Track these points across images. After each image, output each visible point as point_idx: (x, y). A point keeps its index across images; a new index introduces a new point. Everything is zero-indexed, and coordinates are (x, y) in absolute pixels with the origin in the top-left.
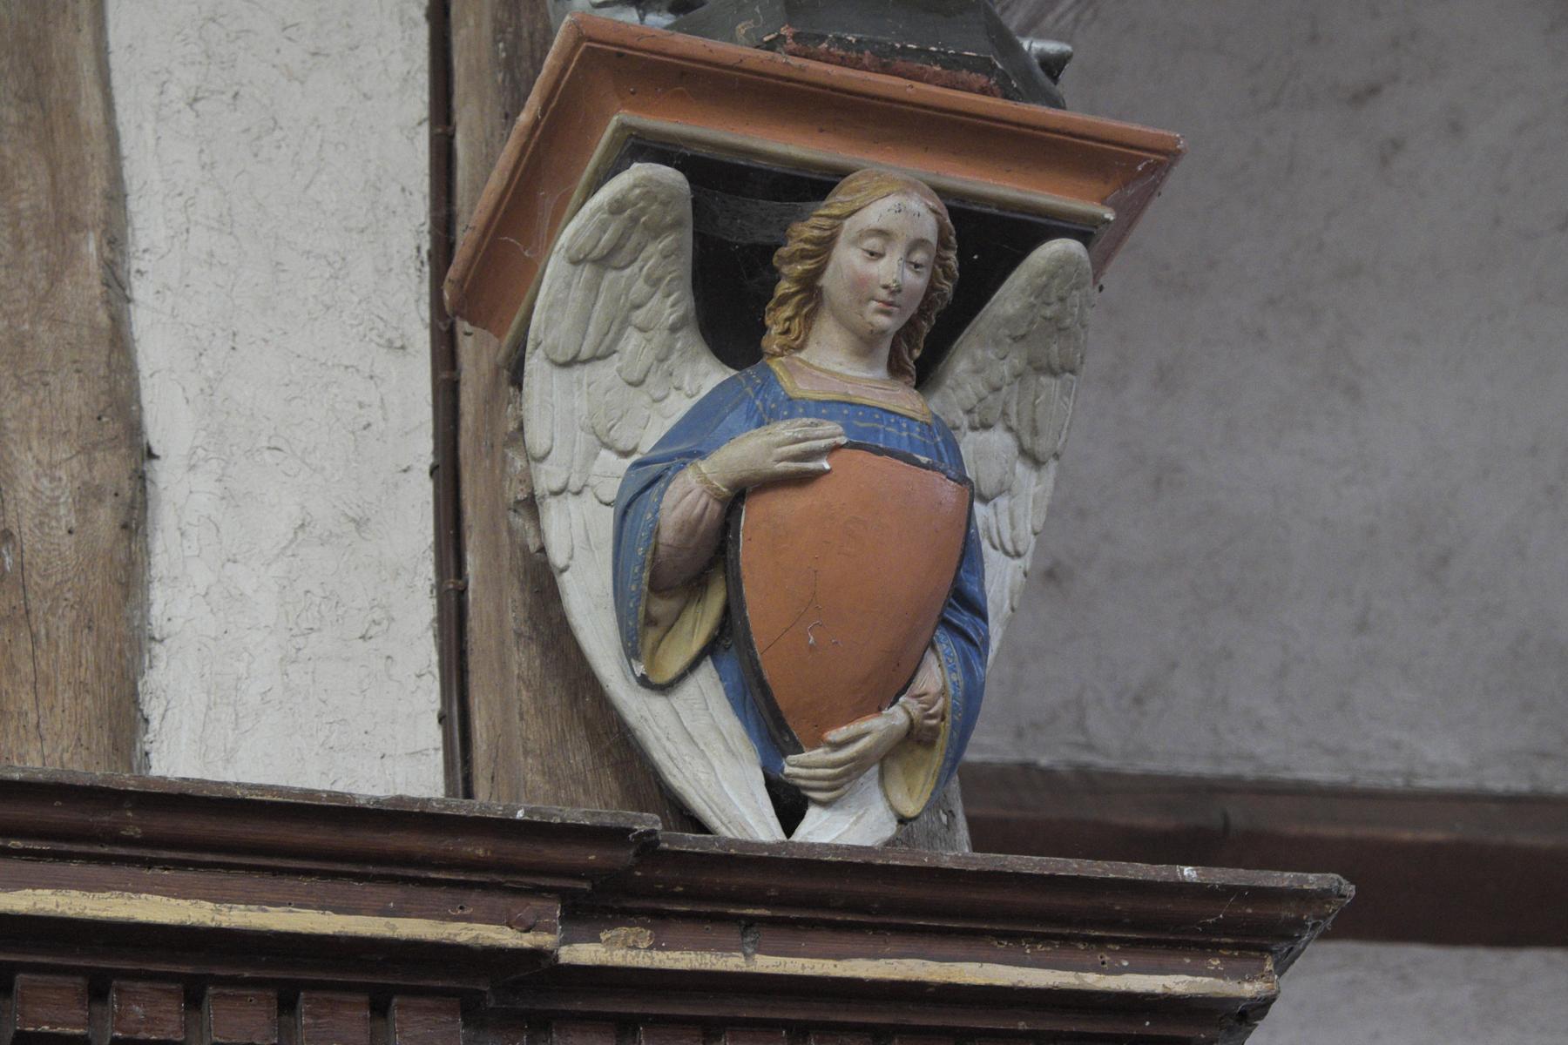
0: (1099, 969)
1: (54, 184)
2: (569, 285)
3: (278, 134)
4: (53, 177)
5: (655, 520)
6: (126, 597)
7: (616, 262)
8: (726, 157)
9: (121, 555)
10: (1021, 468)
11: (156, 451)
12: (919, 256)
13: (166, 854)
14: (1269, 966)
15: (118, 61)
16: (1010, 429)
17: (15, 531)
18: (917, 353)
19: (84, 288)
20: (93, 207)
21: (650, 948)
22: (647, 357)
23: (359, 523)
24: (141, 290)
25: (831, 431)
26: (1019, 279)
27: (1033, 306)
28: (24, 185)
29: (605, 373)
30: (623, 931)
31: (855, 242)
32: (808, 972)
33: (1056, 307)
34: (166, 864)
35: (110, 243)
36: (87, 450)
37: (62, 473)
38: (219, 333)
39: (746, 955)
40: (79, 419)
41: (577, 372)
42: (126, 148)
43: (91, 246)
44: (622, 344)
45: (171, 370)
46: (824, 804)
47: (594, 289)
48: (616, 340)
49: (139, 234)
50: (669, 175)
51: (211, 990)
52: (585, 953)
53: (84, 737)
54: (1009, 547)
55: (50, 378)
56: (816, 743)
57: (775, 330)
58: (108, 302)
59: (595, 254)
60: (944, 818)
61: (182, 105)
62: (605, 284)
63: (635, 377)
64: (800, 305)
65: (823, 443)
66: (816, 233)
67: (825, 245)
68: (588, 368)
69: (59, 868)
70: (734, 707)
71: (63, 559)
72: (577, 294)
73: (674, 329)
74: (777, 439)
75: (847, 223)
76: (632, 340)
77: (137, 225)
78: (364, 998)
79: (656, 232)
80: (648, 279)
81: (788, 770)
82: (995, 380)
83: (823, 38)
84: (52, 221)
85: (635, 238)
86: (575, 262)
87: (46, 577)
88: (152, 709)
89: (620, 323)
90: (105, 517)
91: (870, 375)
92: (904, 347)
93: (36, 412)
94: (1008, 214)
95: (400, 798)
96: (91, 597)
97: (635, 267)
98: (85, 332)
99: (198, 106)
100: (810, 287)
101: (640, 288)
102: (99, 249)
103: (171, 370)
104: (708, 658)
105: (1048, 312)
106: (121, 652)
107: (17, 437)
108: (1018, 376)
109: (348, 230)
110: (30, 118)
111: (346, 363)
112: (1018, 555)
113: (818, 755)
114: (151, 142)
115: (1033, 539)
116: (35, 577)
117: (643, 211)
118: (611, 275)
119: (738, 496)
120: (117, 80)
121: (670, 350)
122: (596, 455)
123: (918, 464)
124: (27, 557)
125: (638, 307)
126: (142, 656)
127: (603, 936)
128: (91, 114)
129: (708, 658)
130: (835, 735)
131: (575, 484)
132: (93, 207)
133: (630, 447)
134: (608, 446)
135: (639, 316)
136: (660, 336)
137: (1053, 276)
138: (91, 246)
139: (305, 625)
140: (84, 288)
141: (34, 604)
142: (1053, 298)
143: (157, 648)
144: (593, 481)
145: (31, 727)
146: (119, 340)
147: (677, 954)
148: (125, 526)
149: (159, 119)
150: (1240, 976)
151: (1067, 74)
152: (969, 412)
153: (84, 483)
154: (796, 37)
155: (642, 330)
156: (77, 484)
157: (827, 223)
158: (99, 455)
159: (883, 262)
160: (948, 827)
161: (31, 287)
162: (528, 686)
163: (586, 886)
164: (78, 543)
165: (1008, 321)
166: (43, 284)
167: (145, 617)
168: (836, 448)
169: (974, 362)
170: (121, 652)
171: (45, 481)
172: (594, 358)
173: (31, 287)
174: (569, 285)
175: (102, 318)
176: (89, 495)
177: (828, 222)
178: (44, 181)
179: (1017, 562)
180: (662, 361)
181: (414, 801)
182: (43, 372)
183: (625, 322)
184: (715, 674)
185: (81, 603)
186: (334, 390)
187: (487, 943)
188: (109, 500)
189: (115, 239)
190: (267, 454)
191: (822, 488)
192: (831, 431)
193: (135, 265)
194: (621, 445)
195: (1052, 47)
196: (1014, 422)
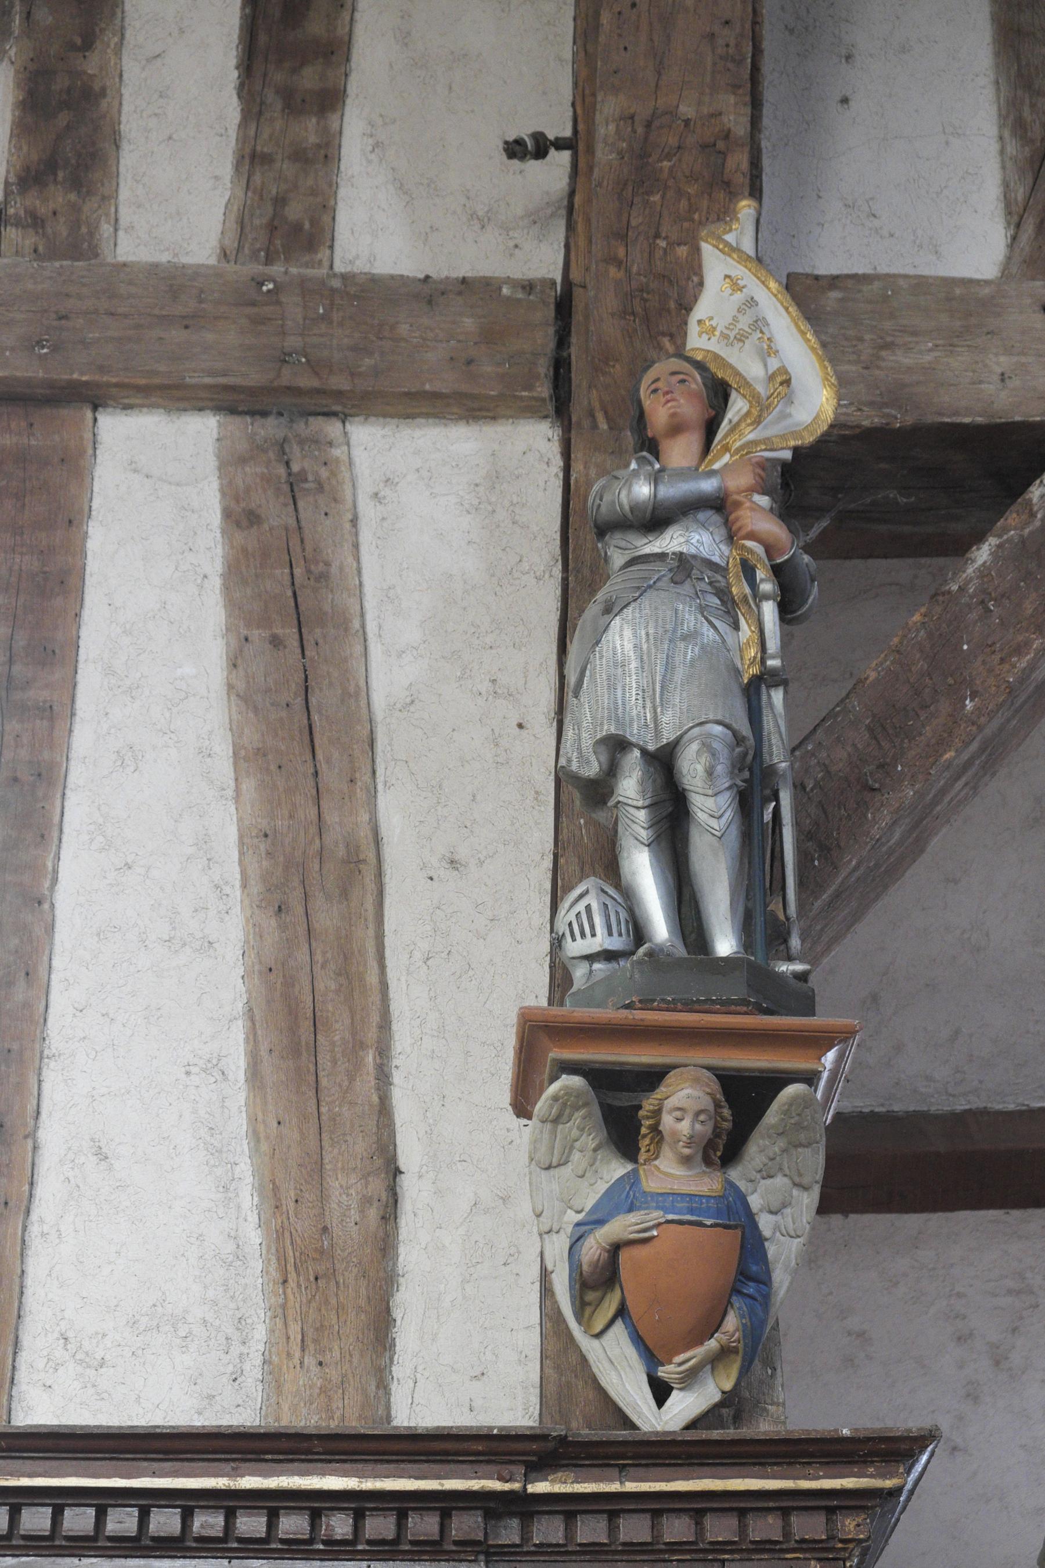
0: (806, 1478)
1: (352, 1023)
2: (542, 1132)
3: (471, 973)
4: (352, 1019)
5: (579, 1260)
6: (384, 1256)
7: (561, 1121)
8: (610, 1067)
9: (381, 1234)
10: (795, 1192)
11: (403, 1170)
12: (702, 1117)
13: (337, 1457)
14: (901, 1470)
15: (390, 941)
16: (785, 1175)
17: (329, 1226)
18: (719, 1154)
19: (366, 1085)
20: (372, 1035)
21: (572, 1483)
22: (584, 1164)
23: (504, 1200)
24: (397, 1078)
25: (656, 1215)
26: (775, 1106)
27: (783, 1119)
28: (337, 1026)
29: (566, 1171)
30: (560, 1474)
31: (670, 1112)
32: (652, 1490)
33: (797, 1118)
34: (338, 1461)
35: (380, 1053)
36: (365, 1177)
37: (352, 1191)
38: (435, 1097)
39: (621, 1483)
40: (362, 1159)
41: (552, 1172)
42: (392, 994)
43: (370, 1058)
44: (572, 1157)
45: (411, 1122)
46: (681, 1389)
47: (554, 1133)
48: (569, 1156)
49: (397, 1043)
50: (576, 1081)
51: (368, 1513)
52: (541, 1487)
53: (361, 1336)
54: (792, 1233)
55: (348, 1138)
56: (670, 1363)
57: (643, 1150)
58: (378, 1089)
59: (551, 1118)
60: (770, 1372)
61: (421, 963)
62: (559, 1130)
63: (580, 1173)
64: (652, 1139)
65: (651, 1223)
66: (652, 1107)
67: (657, 1113)
68: (557, 1170)
69: (290, 1466)
70: (632, 1341)
71: (352, 1240)
72: (546, 1136)
73: (595, 1150)
74: (628, 1223)
75: (666, 1102)
76: (576, 1156)
77: (396, 1039)
78: (438, 1513)
79: (577, 1108)
80: (578, 1128)
81: (659, 1374)
82: (771, 1155)
83: (654, 1001)
84: (351, 1045)
85: (568, 1111)
86: (543, 1122)
87: (343, 1251)
88: (397, 1314)
89: (569, 1148)
90: (373, 1214)
91: (690, 1173)
92: (711, 1152)
93: (340, 1157)
94: (765, 1075)
95: (438, 1427)
96: (365, 1259)
97: (572, 1122)
98: (367, 1107)
99: (429, 963)
100: (655, 1129)
101: (575, 1133)
102: (374, 1059)
103: (411, 1122)
104: (620, 1319)
105: (793, 1121)
106: (381, 1287)
107: (331, 1173)
108: (784, 1151)
109: (506, 1026)
110: (341, 985)
111: (502, 1106)
112: (799, 1237)
113: (670, 1368)
114: (404, 987)
115: (808, 1226)
116: (339, 1251)
117: (568, 1100)
118: (560, 1127)
119: (616, 1248)
120: (388, 953)
121: (595, 1160)
122: (565, 1212)
123: (705, 1226)
124: (335, 1240)
125: (577, 1140)
126: (393, 1285)
127: (550, 1478)
128: (372, 978)
129: (620, 1319)
130: (678, 1359)
131: (555, 1228)
132: (372, 1035)
133: (580, 1209)
134: (570, 1208)
135: (577, 1144)
136: (589, 1154)
137: (791, 1105)
138: (370, 1058)
139: (474, 1261)
140: (366, 1085)
141: (337, 1266)
142: (794, 1114)
143: (401, 1280)
144: (564, 1226)
145: (335, 1333)
146: (384, 1110)
147: (586, 1485)
148: (383, 1218)
149: (408, 974)
150: (884, 1476)
151: (812, 978)
152: (760, 1171)
153: (364, 1196)
154: (640, 1001)
155: (581, 1151)
156: (360, 1197)
157: (657, 1102)
158: (370, 1179)
159: (683, 1123)
160: (772, 1376)
161: (340, 1086)
162: (550, 1320)
163: (534, 1458)
164: (360, 1229)
165: (773, 1126)
166: (346, 1083)
167: (395, 1264)
168: (659, 1224)
169: (759, 1146)
170: (381, 1287)
171: (344, 1196)
172: (559, 1165)
173: (340, 1086)
174: (542, 1132)
175: (375, 1099)
176: (366, 1201)
177: (657, 1102)
178: (348, 1022)
179: (799, 1240)
180: (591, 1165)
181: (444, 1428)
182: (344, 1134)
183: (572, 1148)
184: (623, 1326)
185: (360, 1263)
186: (495, 1123)
187: (488, 1489)
188: (376, 1204)
189: (384, 1050)
190: (459, 1164)
191: (655, 1242)
192: (656, 1215)
193: (395, 1062)
194: (575, 1208)
195: (799, 967)
196: (787, 1172)
